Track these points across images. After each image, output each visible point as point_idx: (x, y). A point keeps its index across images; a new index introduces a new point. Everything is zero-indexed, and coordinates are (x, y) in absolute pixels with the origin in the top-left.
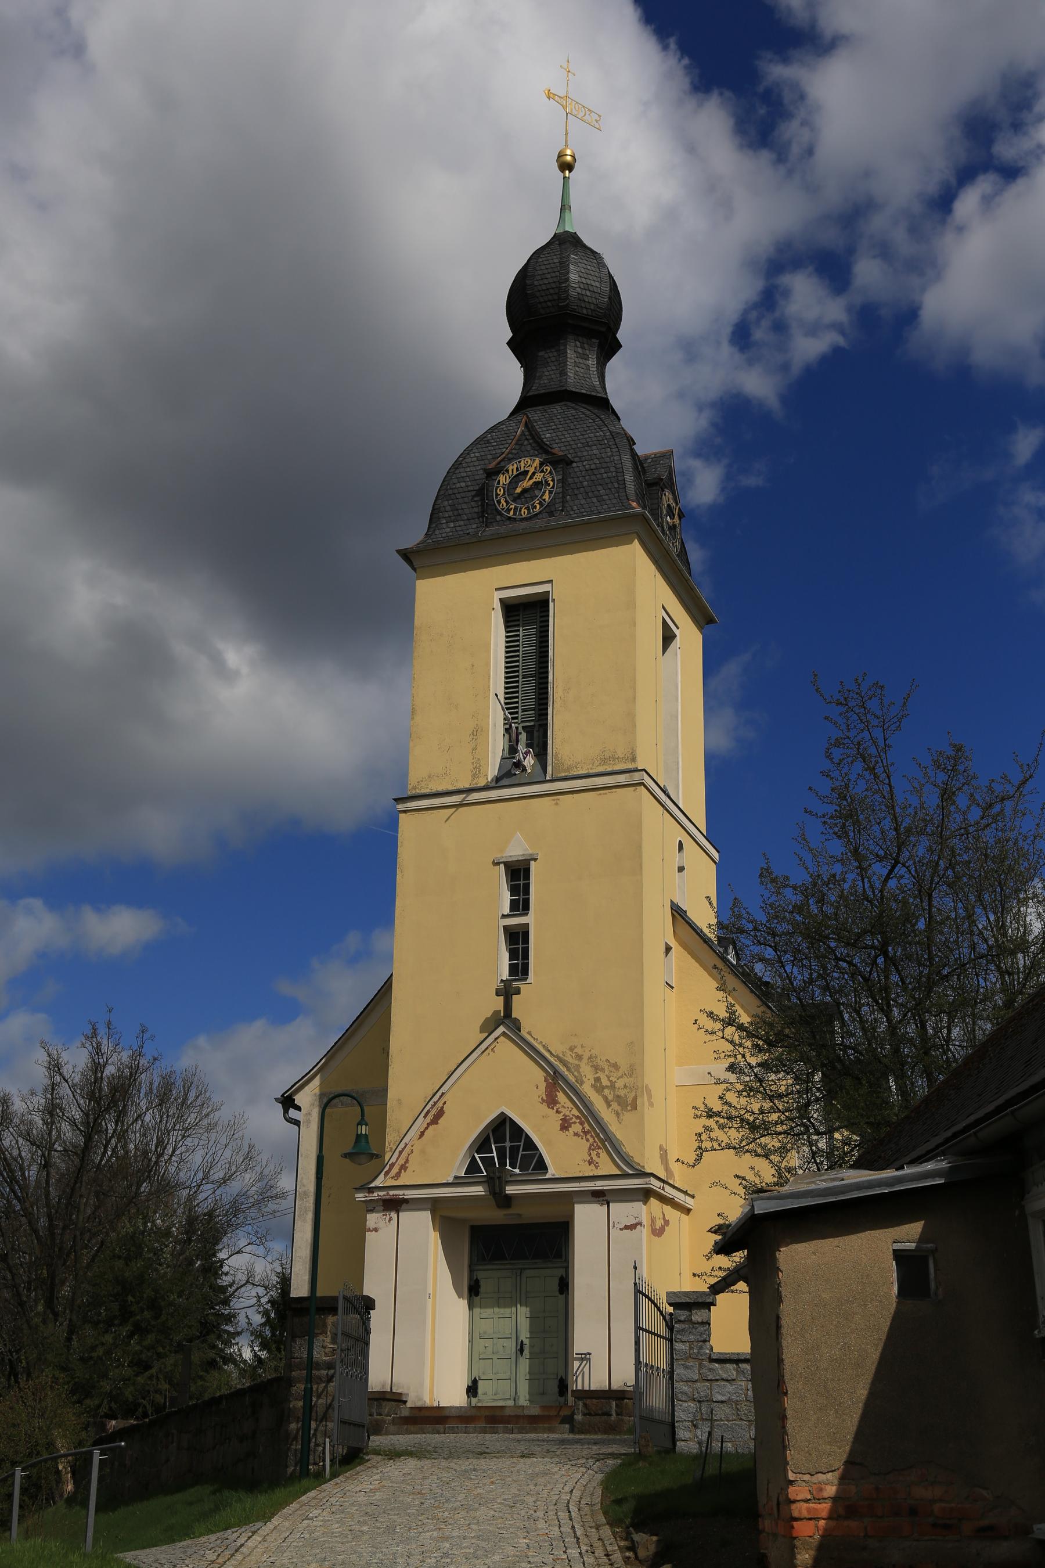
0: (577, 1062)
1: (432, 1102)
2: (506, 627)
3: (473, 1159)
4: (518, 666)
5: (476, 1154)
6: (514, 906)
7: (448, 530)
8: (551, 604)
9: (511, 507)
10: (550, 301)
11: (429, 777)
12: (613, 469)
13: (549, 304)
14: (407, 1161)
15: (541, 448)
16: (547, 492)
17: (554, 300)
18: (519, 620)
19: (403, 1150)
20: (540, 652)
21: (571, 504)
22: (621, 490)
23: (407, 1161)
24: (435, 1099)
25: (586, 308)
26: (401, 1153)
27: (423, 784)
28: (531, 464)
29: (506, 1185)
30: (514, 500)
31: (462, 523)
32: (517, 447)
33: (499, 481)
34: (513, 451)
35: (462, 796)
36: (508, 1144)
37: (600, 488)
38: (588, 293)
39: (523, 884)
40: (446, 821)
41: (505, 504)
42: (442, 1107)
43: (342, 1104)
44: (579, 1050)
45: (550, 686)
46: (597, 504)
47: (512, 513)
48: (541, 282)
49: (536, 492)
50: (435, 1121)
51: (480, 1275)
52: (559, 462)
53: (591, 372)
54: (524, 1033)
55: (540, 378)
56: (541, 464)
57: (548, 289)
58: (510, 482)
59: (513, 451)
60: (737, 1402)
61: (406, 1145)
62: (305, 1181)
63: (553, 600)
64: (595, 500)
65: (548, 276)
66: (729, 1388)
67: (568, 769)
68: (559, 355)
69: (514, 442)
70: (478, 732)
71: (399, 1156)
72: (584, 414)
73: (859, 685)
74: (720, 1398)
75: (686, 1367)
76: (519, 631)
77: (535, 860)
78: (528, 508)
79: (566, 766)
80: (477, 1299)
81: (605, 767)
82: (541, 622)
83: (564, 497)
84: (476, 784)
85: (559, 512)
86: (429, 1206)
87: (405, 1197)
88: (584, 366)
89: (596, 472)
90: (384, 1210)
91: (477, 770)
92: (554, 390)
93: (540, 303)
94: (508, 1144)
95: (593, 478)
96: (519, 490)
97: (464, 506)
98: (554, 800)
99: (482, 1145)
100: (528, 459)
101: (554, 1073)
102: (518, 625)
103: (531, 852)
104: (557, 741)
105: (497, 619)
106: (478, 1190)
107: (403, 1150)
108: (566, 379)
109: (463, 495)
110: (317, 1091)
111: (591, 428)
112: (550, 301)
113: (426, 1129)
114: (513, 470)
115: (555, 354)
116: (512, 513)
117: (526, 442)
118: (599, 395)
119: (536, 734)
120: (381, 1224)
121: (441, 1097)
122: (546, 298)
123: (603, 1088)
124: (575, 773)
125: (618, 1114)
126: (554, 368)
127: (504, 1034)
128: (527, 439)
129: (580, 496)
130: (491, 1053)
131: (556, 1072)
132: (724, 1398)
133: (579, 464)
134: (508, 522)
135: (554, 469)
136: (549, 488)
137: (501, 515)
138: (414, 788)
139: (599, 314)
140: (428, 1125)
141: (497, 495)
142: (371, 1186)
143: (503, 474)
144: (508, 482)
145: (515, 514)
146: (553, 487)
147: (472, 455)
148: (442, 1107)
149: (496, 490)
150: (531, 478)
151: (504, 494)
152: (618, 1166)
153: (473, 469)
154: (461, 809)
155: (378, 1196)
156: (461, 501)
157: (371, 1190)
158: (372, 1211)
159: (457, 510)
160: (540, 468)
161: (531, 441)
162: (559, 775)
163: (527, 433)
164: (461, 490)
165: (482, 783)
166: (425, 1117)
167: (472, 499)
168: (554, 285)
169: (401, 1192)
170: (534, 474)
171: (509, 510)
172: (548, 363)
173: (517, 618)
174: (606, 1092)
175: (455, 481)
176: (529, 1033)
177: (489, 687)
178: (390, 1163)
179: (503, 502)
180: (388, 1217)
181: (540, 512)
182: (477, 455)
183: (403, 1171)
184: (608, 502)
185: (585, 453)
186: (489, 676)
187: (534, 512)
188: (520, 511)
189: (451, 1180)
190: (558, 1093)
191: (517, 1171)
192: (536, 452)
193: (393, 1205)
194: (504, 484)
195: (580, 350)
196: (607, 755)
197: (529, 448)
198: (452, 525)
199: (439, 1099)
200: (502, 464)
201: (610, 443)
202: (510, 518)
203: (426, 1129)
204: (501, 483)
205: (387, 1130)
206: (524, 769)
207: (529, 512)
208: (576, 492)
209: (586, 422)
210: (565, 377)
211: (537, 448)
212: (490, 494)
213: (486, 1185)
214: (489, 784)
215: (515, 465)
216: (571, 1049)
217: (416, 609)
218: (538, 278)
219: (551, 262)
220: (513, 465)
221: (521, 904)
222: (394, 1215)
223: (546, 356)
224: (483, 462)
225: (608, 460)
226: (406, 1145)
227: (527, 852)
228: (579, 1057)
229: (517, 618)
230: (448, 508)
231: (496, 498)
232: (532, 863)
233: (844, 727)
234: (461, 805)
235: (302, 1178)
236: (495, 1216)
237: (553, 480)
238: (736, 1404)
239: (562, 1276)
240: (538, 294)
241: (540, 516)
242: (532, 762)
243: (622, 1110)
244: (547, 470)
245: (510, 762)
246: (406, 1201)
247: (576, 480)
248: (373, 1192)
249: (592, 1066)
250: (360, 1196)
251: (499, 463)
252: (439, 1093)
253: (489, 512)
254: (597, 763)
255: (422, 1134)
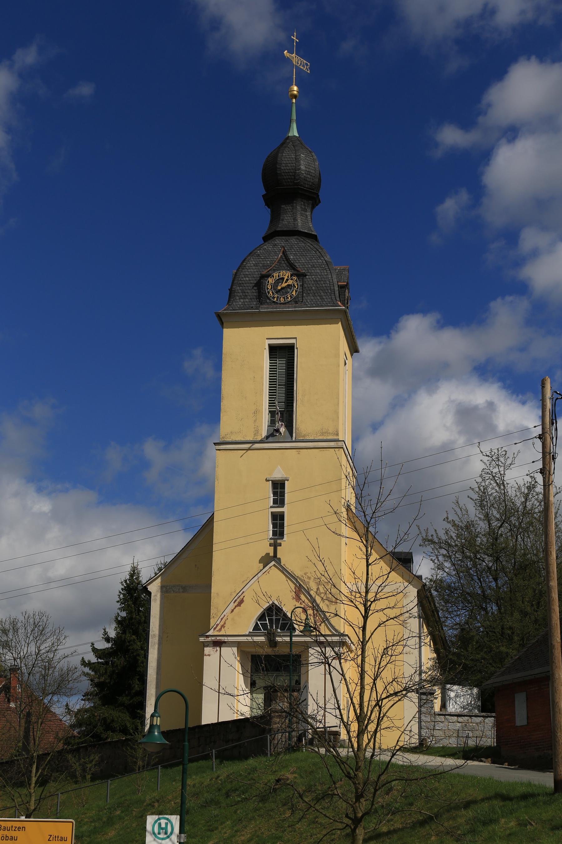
0: (308, 580)
1: (238, 596)
2: (270, 358)
3: (257, 623)
4: (276, 379)
5: (258, 622)
6: (275, 502)
7: (240, 303)
8: (296, 350)
9: (275, 296)
10: (289, 179)
11: (231, 433)
12: (328, 282)
13: (289, 180)
14: (225, 623)
15: (291, 266)
16: (294, 290)
17: (292, 179)
18: (276, 355)
19: (223, 618)
20: (288, 373)
21: (306, 298)
22: (332, 294)
23: (225, 623)
24: (239, 594)
25: (308, 184)
26: (222, 619)
27: (228, 436)
28: (286, 274)
29: (276, 637)
30: (277, 292)
31: (247, 300)
32: (278, 264)
33: (269, 281)
34: (276, 266)
35: (250, 445)
36: (274, 618)
37: (321, 291)
38: (309, 176)
39: (278, 489)
40: (241, 457)
41: (272, 294)
42: (243, 599)
43: (174, 592)
44: (309, 575)
45: (295, 392)
46: (320, 300)
47: (275, 299)
48: (285, 168)
49: (289, 290)
50: (239, 604)
51: (255, 678)
52: (301, 276)
53: (308, 219)
54: (282, 564)
55: (283, 220)
56: (291, 275)
57: (289, 172)
58: (274, 283)
59: (276, 266)
60: (444, 730)
61: (225, 616)
62: (154, 629)
63: (297, 348)
64: (318, 298)
65: (289, 165)
66: (441, 724)
67: (304, 436)
68: (293, 209)
69: (277, 261)
70: (257, 412)
71: (221, 621)
72: (309, 247)
73: (498, 451)
74: (438, 728)
75: (426, 717)
76: (276, 360)
77: (288, 480)
78: (284, 298)
79: (303, 435)
80: (254, 689)
81: (323, 437)
82: (288, 357)
83: (303, 294)
84: (256, 439)
85: (300, 302)
86: (237, 645)
87: (225, 640)
88: (305, 216)
89: (319, 282)
90: (213, 646)
91: (257, 432)
92: (291, 229)
93: (284, 179)
94: (274, 618)
95: (318, 285)
96: (279, 288)
97: (249, 291)
98: (297, 451)
99: (262, 617)
100: (284, 271)
101: (300, 585)
102: (276, 358)
103: (285, 476)
104: (298, 421)
105: (266, 353)
106: (262, 639)
107: (223, 618)
108: (297, 223)
109: (248, 285)
110: (159, 584)
111: (315, 257)
112: (289, 179)
113: (235, 608)
114: (276, 276)
115: (291, 208)
116: (275, 299)
117: (283, 262)
118: (313, 233)
119: (285, 415)
120: (212, 653)
121: (242, 593)
122: (287, 177)
123: (321, 593)
124: (307, 439)
125: (328, 606)
126: (290, 215)
127: (274, 565)
128: (283, 260)
129: (311, 294)
130: (268, 574)
131: (300, 585)
132: (440, 728)
133: (310, 277)
134: (273, 304)
135: (298, 279)
136: (295, 289)
137: (270, 299)
138: (223, 438)
139: (314, 188)
140: (236, 607)
141: (268, 289)
142: (207, 634)
143: (271, 278)
144: (273, 282)
145: (277, 300)
146: (298, 288)
147: (251, 262)
148: (243, 599)
149: (267, 286)
150: (286, 282)
151: (271, 289)
152: (330, 631)
153: (252, 270)
154: (249, 451)
155: (211, 639)
156: (247, 288)
157: (208, 637)
158: (207, 646)
159: (245, 293)
160: (291, 277)
161: (286, 262)
162: (299, 439)
163: (284, 257)
164: (246, 282)
165: (259, 439)
166: (234, 603)
167: (253, 288)
168: (292, 171)
169: (223, 638)
170: (287, 280)
171: (274, 298)
172: (287, 212)
173: (276, 354)
174: (322, 595)
175: (243, 276)
176: (284, 565)
177: (263, 390)
178: (216, 624)
179: (271, 293)
180: (215, 649)
181: (290, 301)
182: (254, 262)
183: (223, 628)
184: (326, 300)
185: (313, 271)
186: (263, 384)
187: (287, 300)
188: (280, 299)
189: (247, 633)
190: (301, 595)
191: (279, 630)
192: (288, 268)
193: (218, 644)
194: (271, 283)
195: (303, 206)
196: (324, 431)
197: (284, 265)
198: (242, 300)
199: (241, 595)
200: (270, 272)
201: (326, 267)
202: (274, 302)
203: (235, 608)
204: (270, 283)
205: (211, 608)
206: (281, 433)
207: (285, 300)
208: (309, 292)
209: (311, 252)
210: (297, 222)
211: (289, 266)
212: (264, 287)
213: (266, 637)
214: (263, 439)
215: (277, 274)
216: (305, 574)
217: (223, 344)
218: (283, 165)
219: (290, 157)
220: (276, 273)
221: (279, 500)
222: (218, 649)
223: (286, 208)
224: (257, 267)
225: (325, 277)
226: (225, 616)
227: (283, 476)
228: (309, 578)
229: (276, 354)
230: (240, 291)
231: (267, 290)
232: (286, 482)
233: (488, 465)
234: (249, 449)
235: (153, 627)
236: (268, 651)
237: (298, 285)
238: (444, 731)
239: (297, 680)
240: (283, 174)
241: (290, 303)
242: (284, 430)
243: (330, 604)
244: (294, 279)
245: (272, 429)
246: (225, 642)
247: (309, 286)
248: (209, 638)
249: (315, 583)
250: (202, 639)
251: (268, 271)
252: (242, 592)
253: (263, 297)
254: (318, 435)
255: (233, 611)
